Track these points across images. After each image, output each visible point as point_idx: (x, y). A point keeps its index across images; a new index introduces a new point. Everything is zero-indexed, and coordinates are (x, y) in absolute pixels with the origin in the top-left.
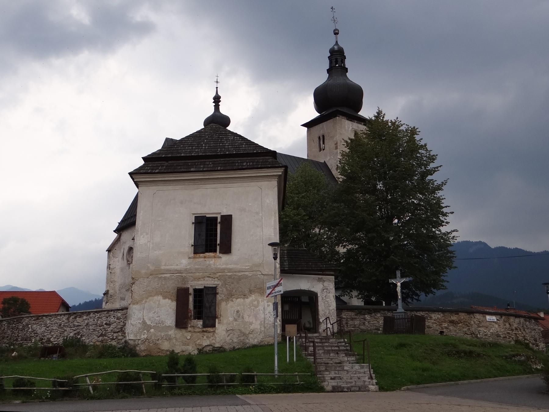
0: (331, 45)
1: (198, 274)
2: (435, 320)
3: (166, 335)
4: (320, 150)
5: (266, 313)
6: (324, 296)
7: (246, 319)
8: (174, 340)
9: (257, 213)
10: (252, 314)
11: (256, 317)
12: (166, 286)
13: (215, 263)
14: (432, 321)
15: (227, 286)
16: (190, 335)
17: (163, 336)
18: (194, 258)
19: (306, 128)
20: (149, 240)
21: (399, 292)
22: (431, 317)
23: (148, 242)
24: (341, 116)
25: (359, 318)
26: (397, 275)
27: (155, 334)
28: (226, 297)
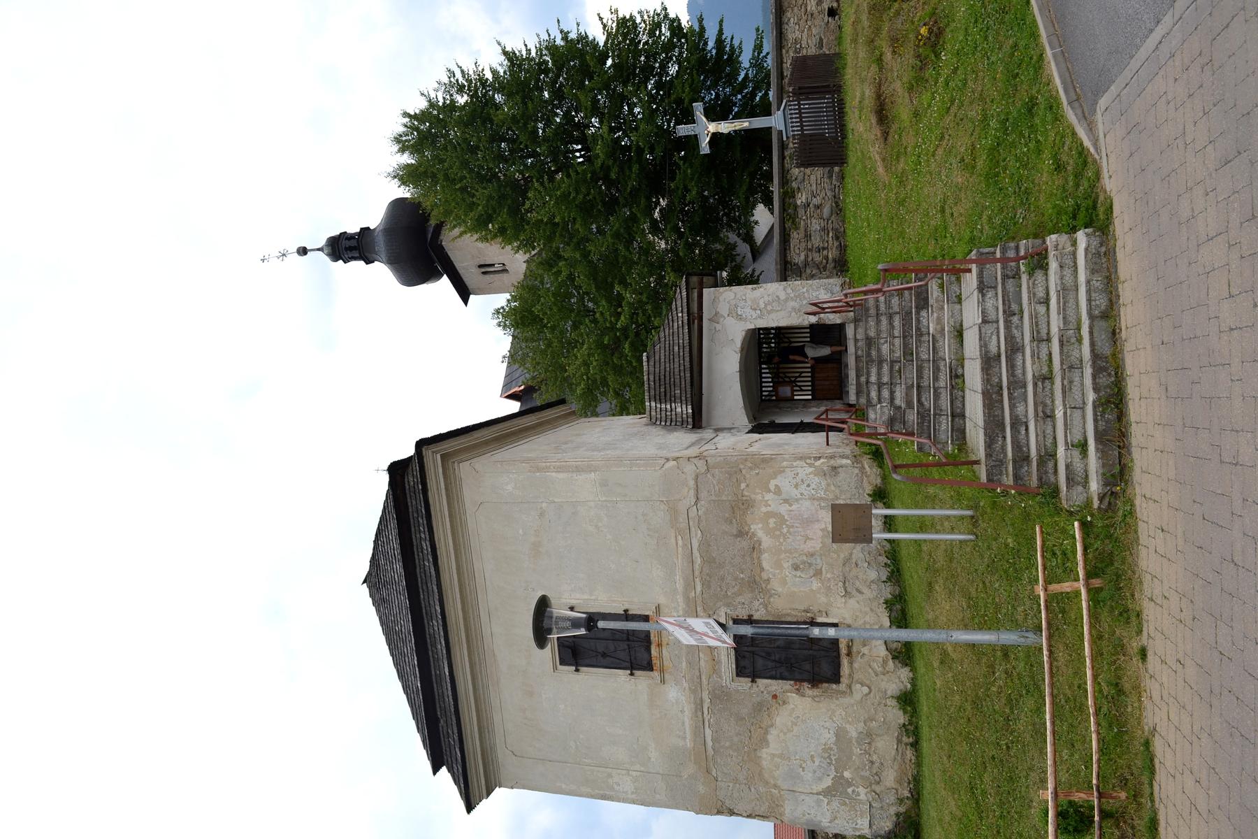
0: (323, 258)
1: (702, 663)
2: (803, 31)
4: (505, 271)
5: (799, 496)
6: (753, 313)
7: (814, 547)
9: (542, 515)
12: (736, 739)
14: (804, 37)
15: (729, 594)
16: (858, 686)
17: (861, 750)
18: (662, 671)
19: (471, 296)
20: (624, 772)
21: (733, 125)
23: (629, 775)
24: (441, 237)
25: (804, 220)
26: (690, 133)
27: (856, 769)
28: (758, 597)
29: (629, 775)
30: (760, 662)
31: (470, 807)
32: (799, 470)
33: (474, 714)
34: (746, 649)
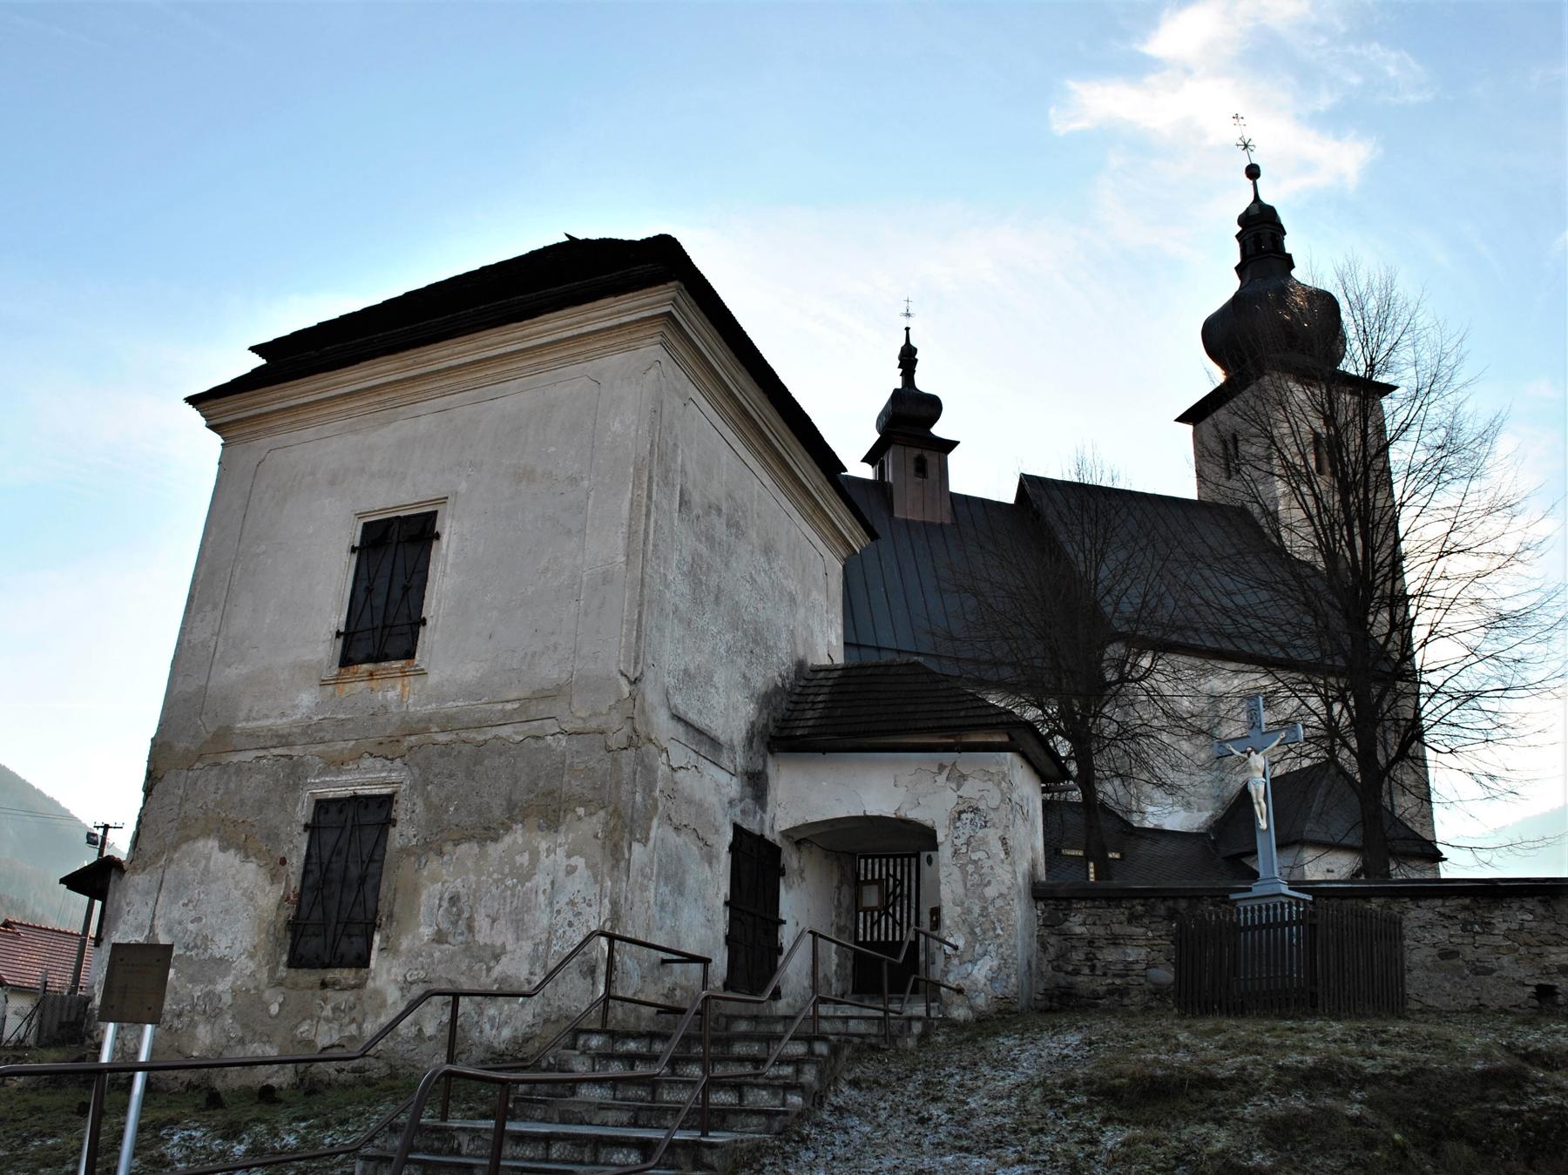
0: (1246, 201)
3: (208, 994)
5: (556, 907)
6: (962, 840)
8: (228, 1017)
9: (574, 480)
10: (508, 910)
11: (519, 926)
13: (403, 697)
21: (1262, 800)
22: (1490, 923)
29: (213, 635)
30: (329, 838)
31: (194, 400)
32: (595, 909)
33: (312, 398)
34: (351, 815)
